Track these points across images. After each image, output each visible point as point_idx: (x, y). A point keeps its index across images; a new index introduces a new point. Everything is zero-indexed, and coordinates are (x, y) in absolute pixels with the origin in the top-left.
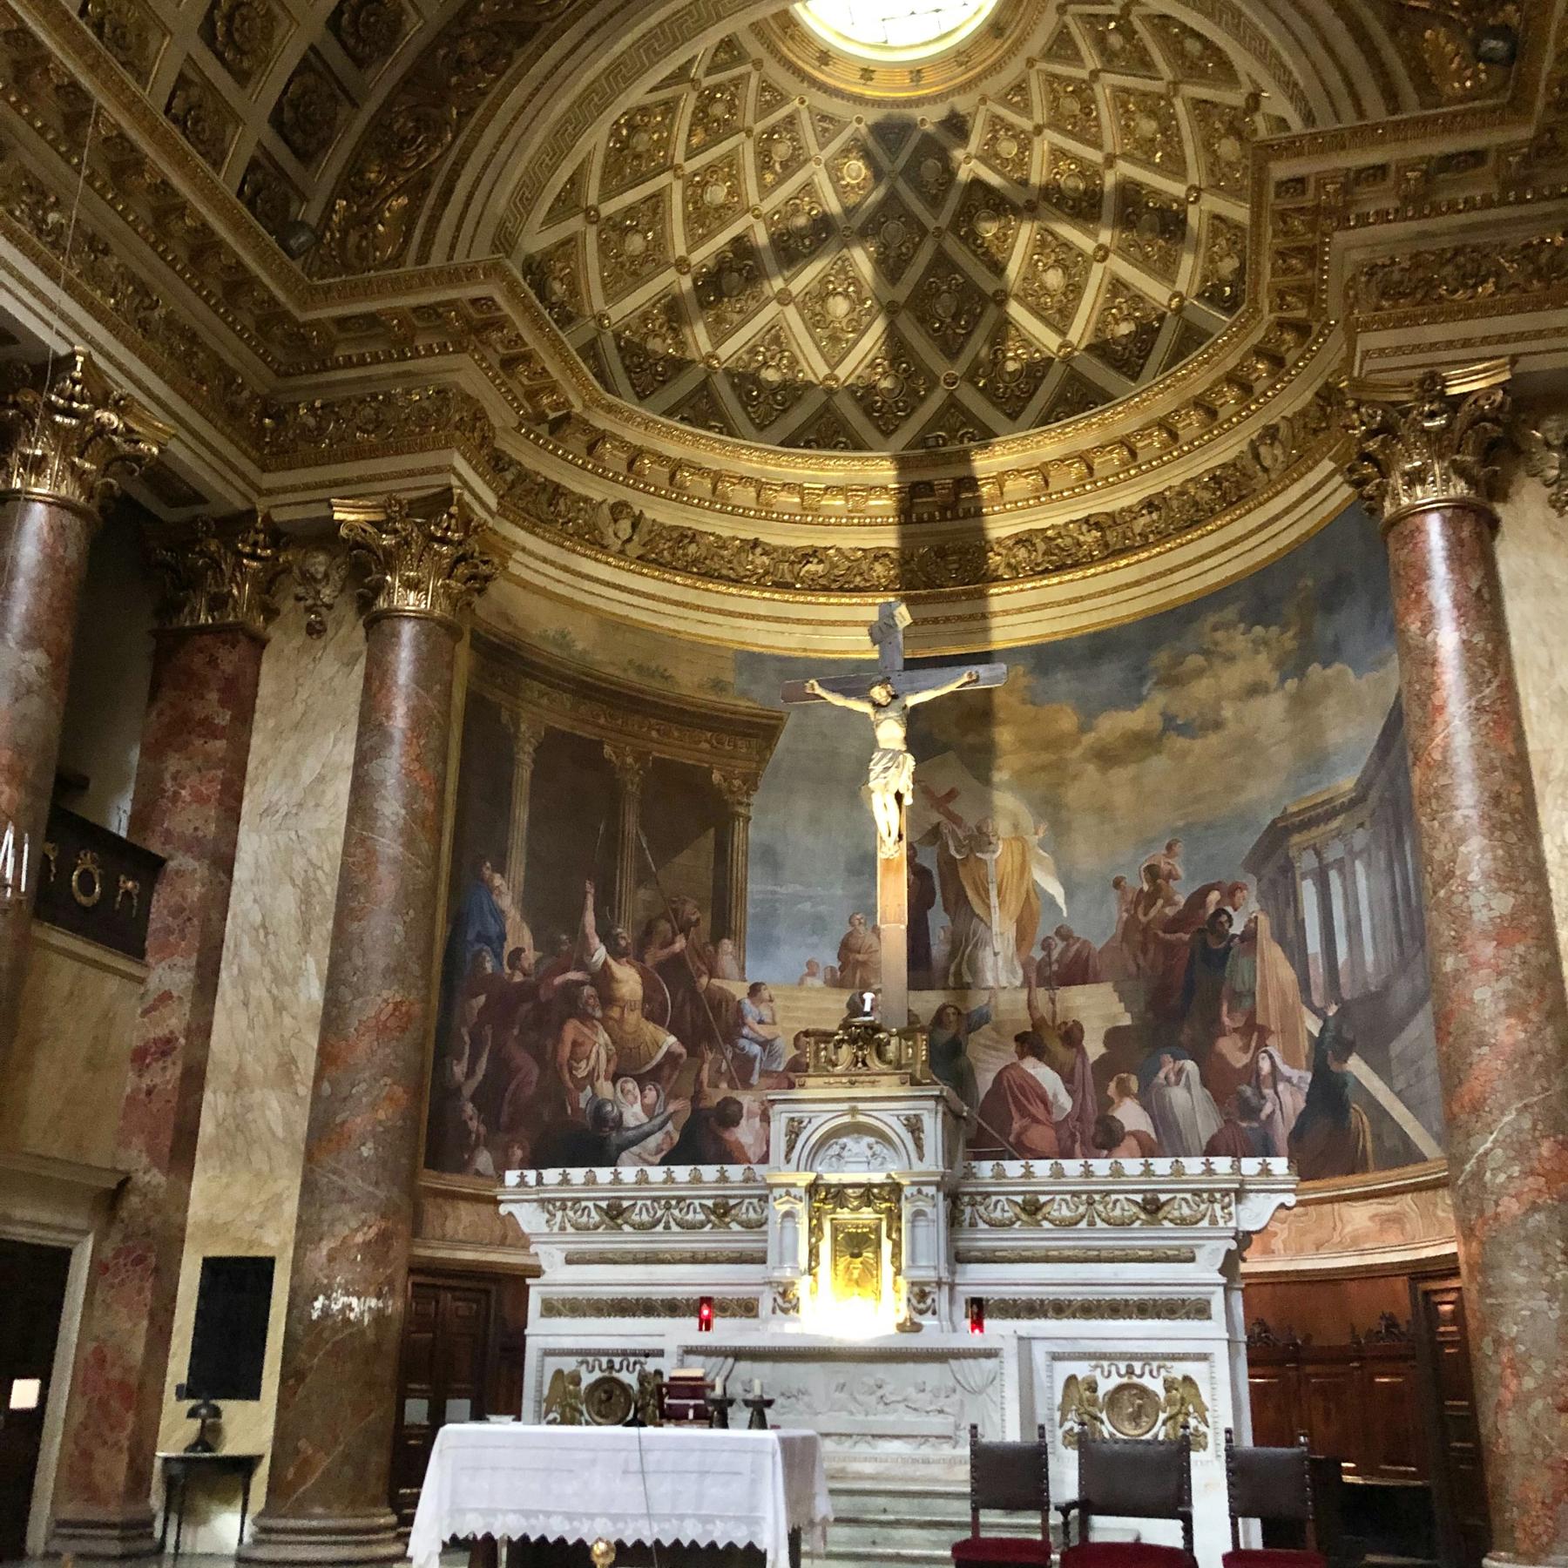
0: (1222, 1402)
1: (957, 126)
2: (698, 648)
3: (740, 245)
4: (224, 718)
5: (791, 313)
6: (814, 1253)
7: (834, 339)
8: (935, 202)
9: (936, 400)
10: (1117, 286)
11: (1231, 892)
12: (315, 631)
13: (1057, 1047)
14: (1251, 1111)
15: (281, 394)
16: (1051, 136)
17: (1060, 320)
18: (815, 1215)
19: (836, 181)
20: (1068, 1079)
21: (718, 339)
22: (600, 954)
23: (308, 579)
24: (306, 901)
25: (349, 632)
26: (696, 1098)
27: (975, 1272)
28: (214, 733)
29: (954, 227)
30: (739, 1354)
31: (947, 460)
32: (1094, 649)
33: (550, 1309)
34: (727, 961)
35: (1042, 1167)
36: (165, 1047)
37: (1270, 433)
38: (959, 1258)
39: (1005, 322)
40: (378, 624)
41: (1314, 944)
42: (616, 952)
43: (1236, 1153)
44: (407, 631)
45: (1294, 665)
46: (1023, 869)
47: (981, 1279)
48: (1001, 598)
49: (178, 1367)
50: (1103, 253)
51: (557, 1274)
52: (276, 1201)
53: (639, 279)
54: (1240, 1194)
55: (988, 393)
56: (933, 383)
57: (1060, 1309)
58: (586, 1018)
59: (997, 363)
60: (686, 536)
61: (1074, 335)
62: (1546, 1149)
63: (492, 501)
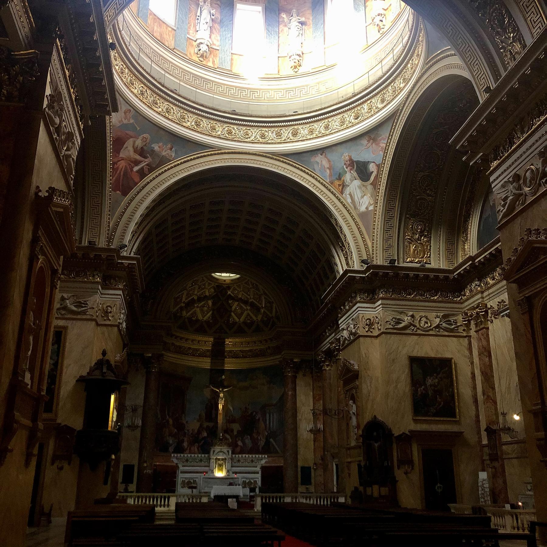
0: (304, 486)
1: (229, 288)
10: (248, 315)
18: (216, 462)
20: (231, 437)
21: (187, 313)
22: (168, 417)
27: (234, 468)
33: (181, 472)
37: (269, 348)
38: (232, 467)
39: (231, 315)
41: (268, 423)
49: (120, 480)
50: (247, 310)
51: (181, 468)
59: (228, 321)
60: (180, 347)
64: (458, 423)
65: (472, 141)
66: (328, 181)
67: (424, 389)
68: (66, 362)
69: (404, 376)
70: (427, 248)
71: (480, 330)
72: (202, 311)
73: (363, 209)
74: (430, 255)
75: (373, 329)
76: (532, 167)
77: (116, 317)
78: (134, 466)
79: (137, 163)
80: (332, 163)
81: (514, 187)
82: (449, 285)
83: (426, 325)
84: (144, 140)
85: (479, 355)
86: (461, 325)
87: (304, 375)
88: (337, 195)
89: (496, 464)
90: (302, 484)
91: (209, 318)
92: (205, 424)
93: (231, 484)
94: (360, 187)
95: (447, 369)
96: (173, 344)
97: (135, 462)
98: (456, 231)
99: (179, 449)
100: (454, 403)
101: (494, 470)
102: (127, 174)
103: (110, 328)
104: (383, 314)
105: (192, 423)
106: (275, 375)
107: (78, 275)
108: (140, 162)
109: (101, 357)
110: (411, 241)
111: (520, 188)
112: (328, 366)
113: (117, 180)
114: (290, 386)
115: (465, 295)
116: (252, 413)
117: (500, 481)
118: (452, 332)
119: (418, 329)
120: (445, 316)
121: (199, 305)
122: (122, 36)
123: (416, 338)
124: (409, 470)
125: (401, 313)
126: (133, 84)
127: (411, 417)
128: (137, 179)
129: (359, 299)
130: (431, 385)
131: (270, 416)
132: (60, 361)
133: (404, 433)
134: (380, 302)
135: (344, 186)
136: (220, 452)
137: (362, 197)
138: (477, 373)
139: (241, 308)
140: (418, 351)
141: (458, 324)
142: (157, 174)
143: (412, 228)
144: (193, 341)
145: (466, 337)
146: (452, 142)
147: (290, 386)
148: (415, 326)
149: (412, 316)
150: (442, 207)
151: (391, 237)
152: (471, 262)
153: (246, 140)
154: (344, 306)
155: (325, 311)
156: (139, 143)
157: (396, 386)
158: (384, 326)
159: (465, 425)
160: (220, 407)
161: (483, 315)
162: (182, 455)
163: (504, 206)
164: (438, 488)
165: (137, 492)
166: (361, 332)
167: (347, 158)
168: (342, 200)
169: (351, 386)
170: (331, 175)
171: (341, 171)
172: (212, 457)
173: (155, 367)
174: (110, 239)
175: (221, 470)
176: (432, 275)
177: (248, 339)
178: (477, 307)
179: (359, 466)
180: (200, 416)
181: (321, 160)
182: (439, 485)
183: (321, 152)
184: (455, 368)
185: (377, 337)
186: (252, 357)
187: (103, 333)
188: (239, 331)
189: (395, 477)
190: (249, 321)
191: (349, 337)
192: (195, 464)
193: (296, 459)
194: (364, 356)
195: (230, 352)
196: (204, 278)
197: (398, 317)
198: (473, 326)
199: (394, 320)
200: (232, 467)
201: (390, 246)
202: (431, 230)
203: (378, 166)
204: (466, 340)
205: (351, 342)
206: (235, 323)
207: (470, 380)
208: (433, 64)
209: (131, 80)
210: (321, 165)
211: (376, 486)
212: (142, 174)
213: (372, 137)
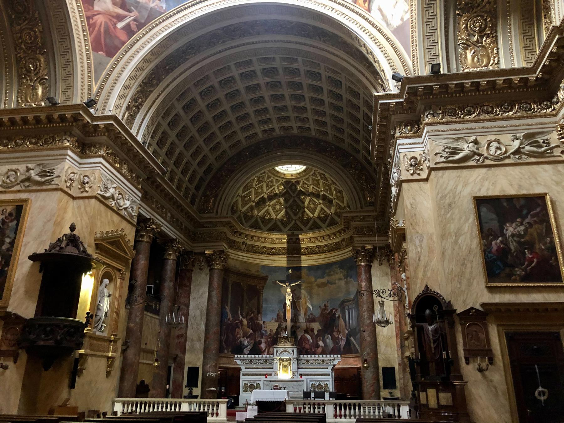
0: (387, 391)
1: (298, 182)
2: (255, 265)
4: (188, 284)
5: (270, 208)
6: (280, 368)
7: (277, 212)
8: (294, 192)
10: (322, 208)
11: (336, 310)
12: (201, 269)
13: (310, 332)
14: (338, 344)
15: (195, 231)
16: (312, 186)
19: (278, 188)
20: (312, 338)
22: (241, 317)
23: (200, 261)
24: (201, 313)
25: (207, 270)
26: (255, 340)
27: (300, 370)
28: (187, 286)
29: (297, 196)
30: (271, 381)
31: (295, 235)
33: (243, 375)
34: (260, 318)
35: (309, 356)
36: (182, 336)
37: (344, 239)
38: (298, 368)
40: (211, 270)
42: (243, 317)
43: (334, 354)
44: (216, 271)
45: (346, 277)
46: (306, 303)
47: (301, 371)
48: (303, 258)
49: (185, 383)
50: (320, 204)
51: (244, 370)
52: (199, 358)
53: (247, 204)
54: (334, 360)
55: (301, 222)
56: (293, 220)
57: (311, 375)
58: (239, 328)
59: (303, 217)
60: (253, 246)
61: (315, 215)
62: (371, 354)
63: (227, 247)
67: (501, 242)
69: (467, 225)
70: (492, 52)
72: (274, 209)
73: (396, 23)
74: (498, 61)
75: (422, 170)
77: (95, 187)
78: (198, 368)
79: (120, 18)
86: (558, 146)
87: (381, 264)
88: (364, 14)
90: (385, 388)
91: (283, 216)
93: (275, 388)
96: (243, 243)
97: (199, 364)
100: (557, 259)
103: (87, 200)
104: (431, 144)
107: (46, 142)
110: (466, 47)
114: (363, 276)
116: (332, 310)
119: (486, 158)
120: (528, 136)
121: (271, 204)
123: (484, 170)
124: (484, 365)
125: (458, 139)
127: (482, 284)
128: (123, 36)
130: (513, 235)
131: (349, 313)
133: (472, 308)
136: (286, 351)
140: (488, 189)
141: (552, 145)
143: (466, 27)
147: (363, 276)
148: (480, 155)
149: (476, 142)
152: (557, 36)
157: (456, 242)
158: (433, 160)
162: (260, 356)
164: (539, 394)
168: (370, 18)
172: (275, 357)
173: (217, 264)
177: (322, 233)
182: (541, 389)
184: (554, 216)
186: (328, 252)
187: (79, 207)
188: (315, 227)
190: (323, 216)
193: (376, 360)
194: (409, 206)
195: (307, 248)
202: (496, 26)
206: (309, 219)
211: (431, 390)
212: (129, 31)
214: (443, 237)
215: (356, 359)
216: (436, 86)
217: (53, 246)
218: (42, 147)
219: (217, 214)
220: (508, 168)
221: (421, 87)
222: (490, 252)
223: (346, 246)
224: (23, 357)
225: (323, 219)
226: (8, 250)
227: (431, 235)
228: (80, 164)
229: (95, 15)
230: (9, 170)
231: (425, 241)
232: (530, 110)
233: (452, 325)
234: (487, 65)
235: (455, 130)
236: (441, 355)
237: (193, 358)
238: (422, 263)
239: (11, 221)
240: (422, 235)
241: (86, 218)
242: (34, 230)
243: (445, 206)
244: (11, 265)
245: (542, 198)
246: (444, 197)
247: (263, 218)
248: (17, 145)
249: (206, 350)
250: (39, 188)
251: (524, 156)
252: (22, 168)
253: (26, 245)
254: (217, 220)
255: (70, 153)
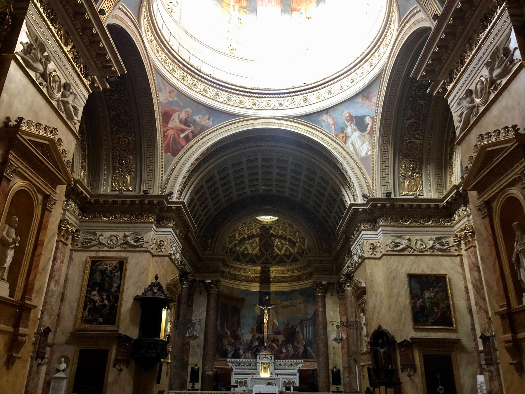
0: (335, 386)
1: (271, 228)
3: (244, 237)
9: (264, 258)
10: (287, 248)
11: (296, 326)
12: (201, 293)
14: (297, 351)
17: (280, 250)
19: (255, 231)
20: (277, 346)
21: (240, 248)
26: (236, 347)
32: (282, 293)
33: (235, 374)
34: (239, 331)
35: (281, 361)
38: (274, 369)
41: (305, 334)
45: (305, 302)
46: (273, 320)
47: (277, 372)
49: (189, 380)
50: (286, 244)
51: (235, 371)
53: (232, 242)
57: (283, 375)
59: (272, 253)
60: (235, 275)
64: (455, 331)
65: (430, 70)
66: (333, 135)
67: (422, 301)
68: (127, 285)
70: (419, 183)
71: (469, 248)
72: (251, 246)
73: (363, 154)
75: (377, 252)
76: (481, 78)
77: (167, 249)
79: (183, 131)
80: (336, 120)
81: (468, 102)
82: (441, 212)
83: (422, 247)
84: (187, 113)
85: (470, 270)
86: (453, 246)
88: (342, 145)
89: (492, 368)
90: (333, 384)
92: (257, 336)
93: (269, 384)
94: (359, 137)
95: (442, 284)
98: (443, 165)
99: (236, 355)
101: (490, 373)
102: (175, 140)
104: (384, 239)
105: (247, 336)
106: (308, 295)
107: (136, 217)
108: (186, 130)
109: (154, 281)
110: (405, 177)
111: (472, 101)
112: (348, 286)
113: (168, 146)
114: (320, 304)
115: (454, 220)
116: (293, 326)
117: (496, 384)
118: (445, 252)
119: (415, 250)
120: (438, 239)
122: (162, 34)
123: (413, 258)
124: (411, 373)
125: (399, 237)
126: (175, 71)
128: (183, 143)
129: (363, 228)
130: (428, 298)
132: (122, 285)
133: (405, 340)
134: (380, 229)
135: (346, 137)
137: (362, 145)
138: (470, 286)
139: (281, 243)
140: (415, 269)
141: (450, 245)
142: (199, 138)
143: (405, 166)
144: (245, 270)
145: (458, 256)
146: (413, 74)
147: (320, 304)
149: (409, 240)
150: (430, 148)
151: (387, 175)
152: (455, 191)
153: (268, 108)
154: (354, 235)
155: (341, 241)
156: (183, 116)
157: (397, 300)
158: (385, 249)
159: (463, 334)
160: (265, 321)
161: (470, 235)
163: (460, 122)
165: (202, 390)
166: (366, 255)
167: (347, 115)
168: (346, 148)
169: (361, 301)
170: (335, 130)
171: (343, 126)
172: (258, 361)
174: (163, 189)
175: (266, 372)
176: (424, 204)
177: (288, 268)
178: (465, 229)
179: (368, 368)
180: (252, 329)
181: (326, 118)
182: (440, 387)
183: (326, 112)
184: (449, 283)
185: (380, 258)
187: (157, 262)
188: (281, 261)
189: (399, 379)
191: (358, 260)
192: (246, 367)
195: (274, 278)
196: (251, 221)
197: (396, 241)
198: (463, 246)
199: (393, 243)
200: (274, 369)
201: (387, 183)
202: (422, 168)
203: (372, 118)
204: (458, 258)
205: (360, 264)
206: (277, 255)
207: (464, 293)
208: (405, 25)
209: (173, 68)
210: (327, 122)
212: (187, 139)
213: (365, 95)
214: (390, 297)
215: (311, 363)
216: (388, 204)
217: (146, 291)
218: (133, 221)
219: (213, 252)
220: (426, 257)
221: (379, 204)
222: (416, 307)
223: (306, 279)
224: (133, 364)
225: (288, 256)
226: (116, 291)
227: (382, 293)
228: (156, 231)
229: (168, 130)
230: (111, 236)
231: (378, 297)
232: (439, 222)
233: (394, 350)
234: (416, 191)
235: (398, 231)
236: (388, 367)
237: (195, 360)
238: (376, 310)
239: (117, 272)
240: (376, 293)
241: (163, 270)
242: (132, 279)
243: (391, 278)
244: (119, 301)
245: (444, 277)
246: (391, 272)
247: (242, 253)
248: (116, 217)
249: (204, 355)
250: (133, 249)
251: (435, 251)
252: (121, 234)
253: (127, 289)
254: (215, 257)
255: (154, 226)
